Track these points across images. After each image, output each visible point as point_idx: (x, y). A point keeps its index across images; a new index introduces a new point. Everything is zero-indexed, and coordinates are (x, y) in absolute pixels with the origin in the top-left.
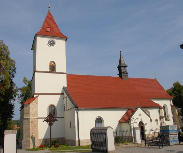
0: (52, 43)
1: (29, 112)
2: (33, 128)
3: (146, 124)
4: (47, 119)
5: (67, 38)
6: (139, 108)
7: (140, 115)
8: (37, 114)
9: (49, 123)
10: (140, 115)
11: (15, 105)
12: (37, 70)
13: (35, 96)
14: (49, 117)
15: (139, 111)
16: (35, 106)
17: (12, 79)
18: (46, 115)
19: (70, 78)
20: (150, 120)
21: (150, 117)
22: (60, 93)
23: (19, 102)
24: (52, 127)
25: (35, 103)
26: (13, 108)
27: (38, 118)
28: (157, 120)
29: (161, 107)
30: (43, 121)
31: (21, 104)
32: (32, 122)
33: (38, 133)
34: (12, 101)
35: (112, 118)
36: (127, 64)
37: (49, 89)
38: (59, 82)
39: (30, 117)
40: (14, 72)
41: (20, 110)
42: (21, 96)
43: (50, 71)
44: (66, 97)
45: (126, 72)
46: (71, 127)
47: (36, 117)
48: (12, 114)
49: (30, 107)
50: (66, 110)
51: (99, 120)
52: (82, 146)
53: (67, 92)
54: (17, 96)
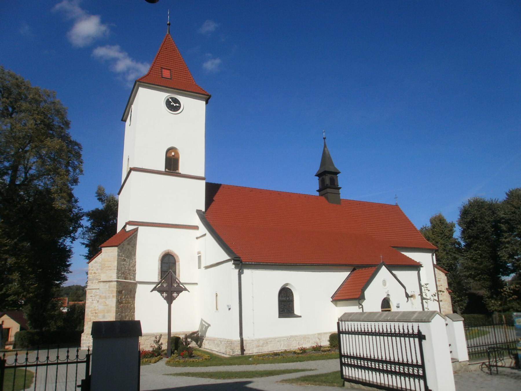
4: (162, 286)
5: (210, 97)
6: (384, 266)
11: (73, 250)
17: (72, 187)
23: (83, 244)
26: (69, 256)
30: (152, 291)
31: (87, 249)
34: (68, 242)
40: (77, 171)
42: (89, 230)
46: (217, 309)
47: (131, 279)
48: (65, 271)
50: (203, 265)
52: (250, 357)
54: (80, 230)
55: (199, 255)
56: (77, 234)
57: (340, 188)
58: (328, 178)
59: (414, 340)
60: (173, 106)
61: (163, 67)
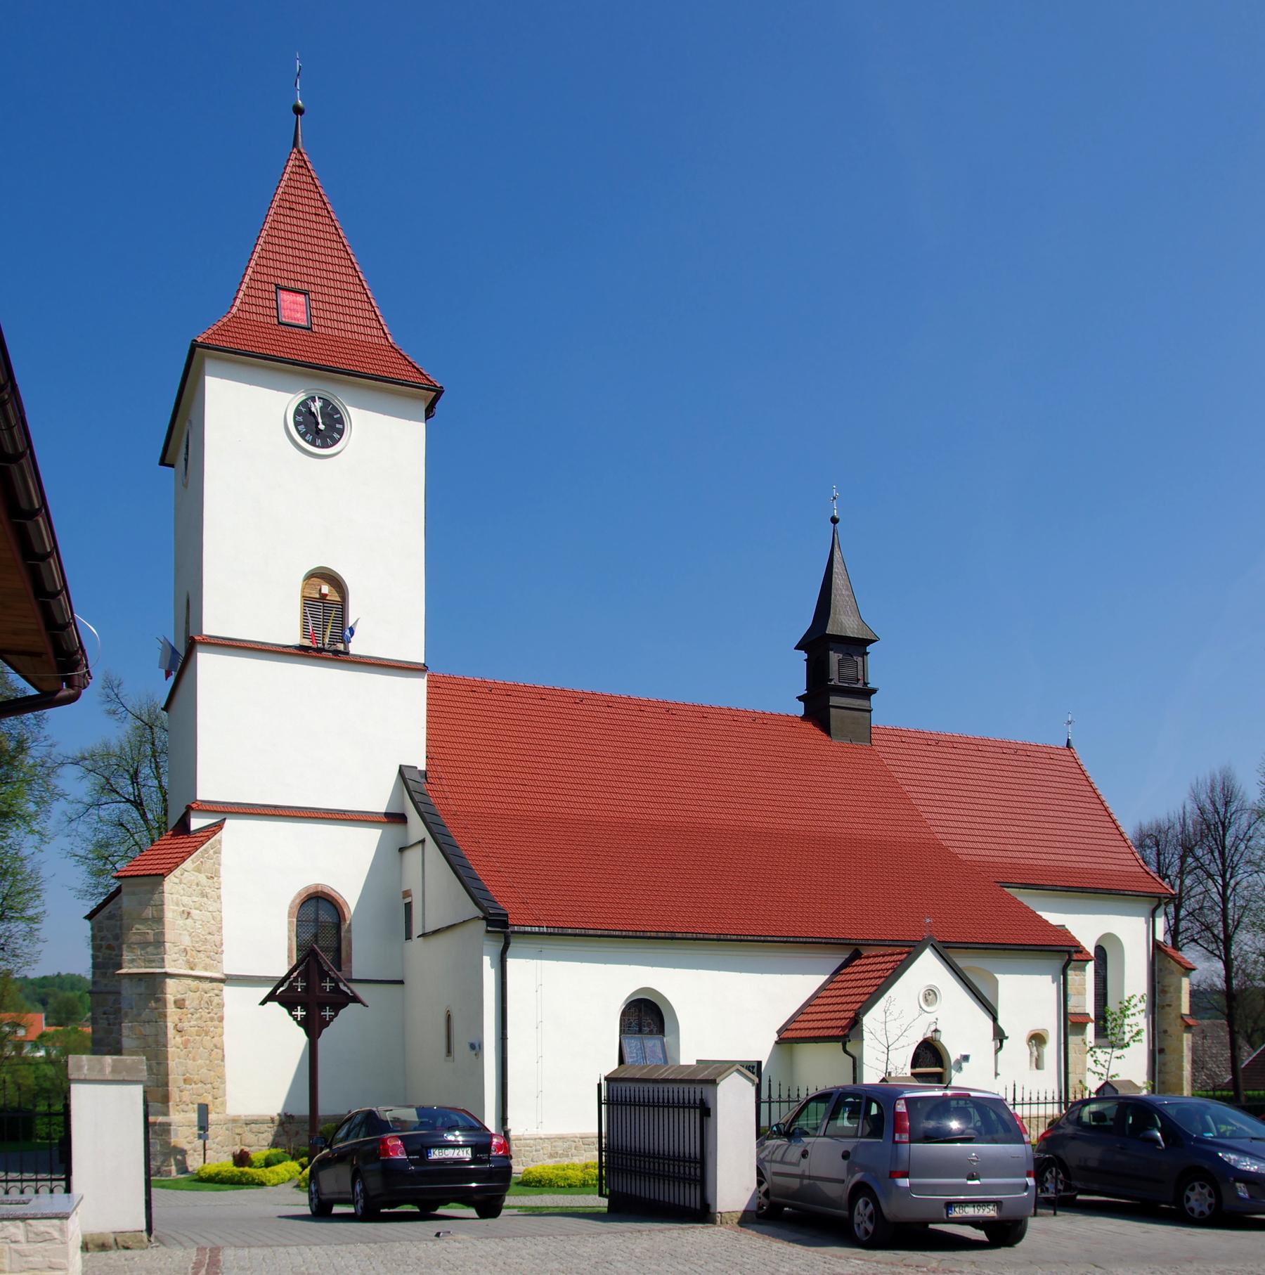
0: (320, 428)
1: (163, 934)
2: (185, 1045)
3: (966, 1058)
4: (291, 988)
5: (439, 392)
7: (931, 995)
8: (218, 949)
9: (300, 1013)
10: (931, 995)
12: (212, 626)
13: (196, 823)
14: (305, 975)
15: (927, 968)
16: (204, 895)
18: (277, 960)
19: (451, 705)
20: (998, 1040)
21: (992, 1012)
22: (382, 808)
24: (321, 1041)
25: (199, 871)
27: (222, 981)
28: (1037, 1039)
29: (1079, 949)
30: (263, 1003)
32: (180, 1004)
33: (222, 1078)
34: (28, 844)
35: (732, 1012)
36: (876, 627)
37: (303, 769)
38: (371, 734)
39: (169, 970)
41: (89, 917)
42: (1123, 1012)
43: (307, 643)
44: (423, 841)
45: (860, 685)
49: (167, 897)
50: (417, 930)
51: (645, 1016)
53: (424, 806)
54: (58, 807)
55: (408, 900)
56: (51, 825)
57: (874, 691)
58: (832, 664)
59: (509, 1207)
60: (320, 428)
61: (284, 283)
